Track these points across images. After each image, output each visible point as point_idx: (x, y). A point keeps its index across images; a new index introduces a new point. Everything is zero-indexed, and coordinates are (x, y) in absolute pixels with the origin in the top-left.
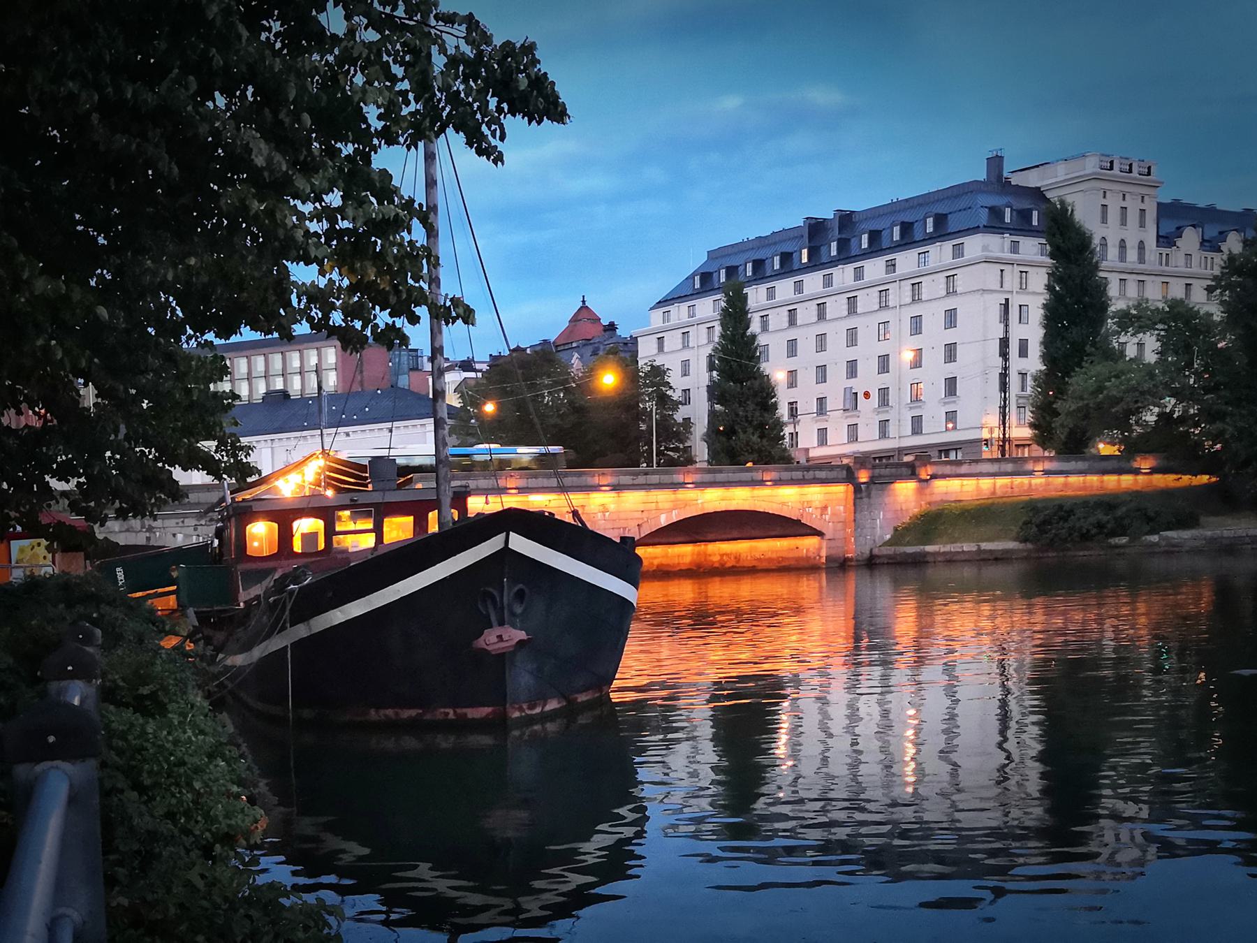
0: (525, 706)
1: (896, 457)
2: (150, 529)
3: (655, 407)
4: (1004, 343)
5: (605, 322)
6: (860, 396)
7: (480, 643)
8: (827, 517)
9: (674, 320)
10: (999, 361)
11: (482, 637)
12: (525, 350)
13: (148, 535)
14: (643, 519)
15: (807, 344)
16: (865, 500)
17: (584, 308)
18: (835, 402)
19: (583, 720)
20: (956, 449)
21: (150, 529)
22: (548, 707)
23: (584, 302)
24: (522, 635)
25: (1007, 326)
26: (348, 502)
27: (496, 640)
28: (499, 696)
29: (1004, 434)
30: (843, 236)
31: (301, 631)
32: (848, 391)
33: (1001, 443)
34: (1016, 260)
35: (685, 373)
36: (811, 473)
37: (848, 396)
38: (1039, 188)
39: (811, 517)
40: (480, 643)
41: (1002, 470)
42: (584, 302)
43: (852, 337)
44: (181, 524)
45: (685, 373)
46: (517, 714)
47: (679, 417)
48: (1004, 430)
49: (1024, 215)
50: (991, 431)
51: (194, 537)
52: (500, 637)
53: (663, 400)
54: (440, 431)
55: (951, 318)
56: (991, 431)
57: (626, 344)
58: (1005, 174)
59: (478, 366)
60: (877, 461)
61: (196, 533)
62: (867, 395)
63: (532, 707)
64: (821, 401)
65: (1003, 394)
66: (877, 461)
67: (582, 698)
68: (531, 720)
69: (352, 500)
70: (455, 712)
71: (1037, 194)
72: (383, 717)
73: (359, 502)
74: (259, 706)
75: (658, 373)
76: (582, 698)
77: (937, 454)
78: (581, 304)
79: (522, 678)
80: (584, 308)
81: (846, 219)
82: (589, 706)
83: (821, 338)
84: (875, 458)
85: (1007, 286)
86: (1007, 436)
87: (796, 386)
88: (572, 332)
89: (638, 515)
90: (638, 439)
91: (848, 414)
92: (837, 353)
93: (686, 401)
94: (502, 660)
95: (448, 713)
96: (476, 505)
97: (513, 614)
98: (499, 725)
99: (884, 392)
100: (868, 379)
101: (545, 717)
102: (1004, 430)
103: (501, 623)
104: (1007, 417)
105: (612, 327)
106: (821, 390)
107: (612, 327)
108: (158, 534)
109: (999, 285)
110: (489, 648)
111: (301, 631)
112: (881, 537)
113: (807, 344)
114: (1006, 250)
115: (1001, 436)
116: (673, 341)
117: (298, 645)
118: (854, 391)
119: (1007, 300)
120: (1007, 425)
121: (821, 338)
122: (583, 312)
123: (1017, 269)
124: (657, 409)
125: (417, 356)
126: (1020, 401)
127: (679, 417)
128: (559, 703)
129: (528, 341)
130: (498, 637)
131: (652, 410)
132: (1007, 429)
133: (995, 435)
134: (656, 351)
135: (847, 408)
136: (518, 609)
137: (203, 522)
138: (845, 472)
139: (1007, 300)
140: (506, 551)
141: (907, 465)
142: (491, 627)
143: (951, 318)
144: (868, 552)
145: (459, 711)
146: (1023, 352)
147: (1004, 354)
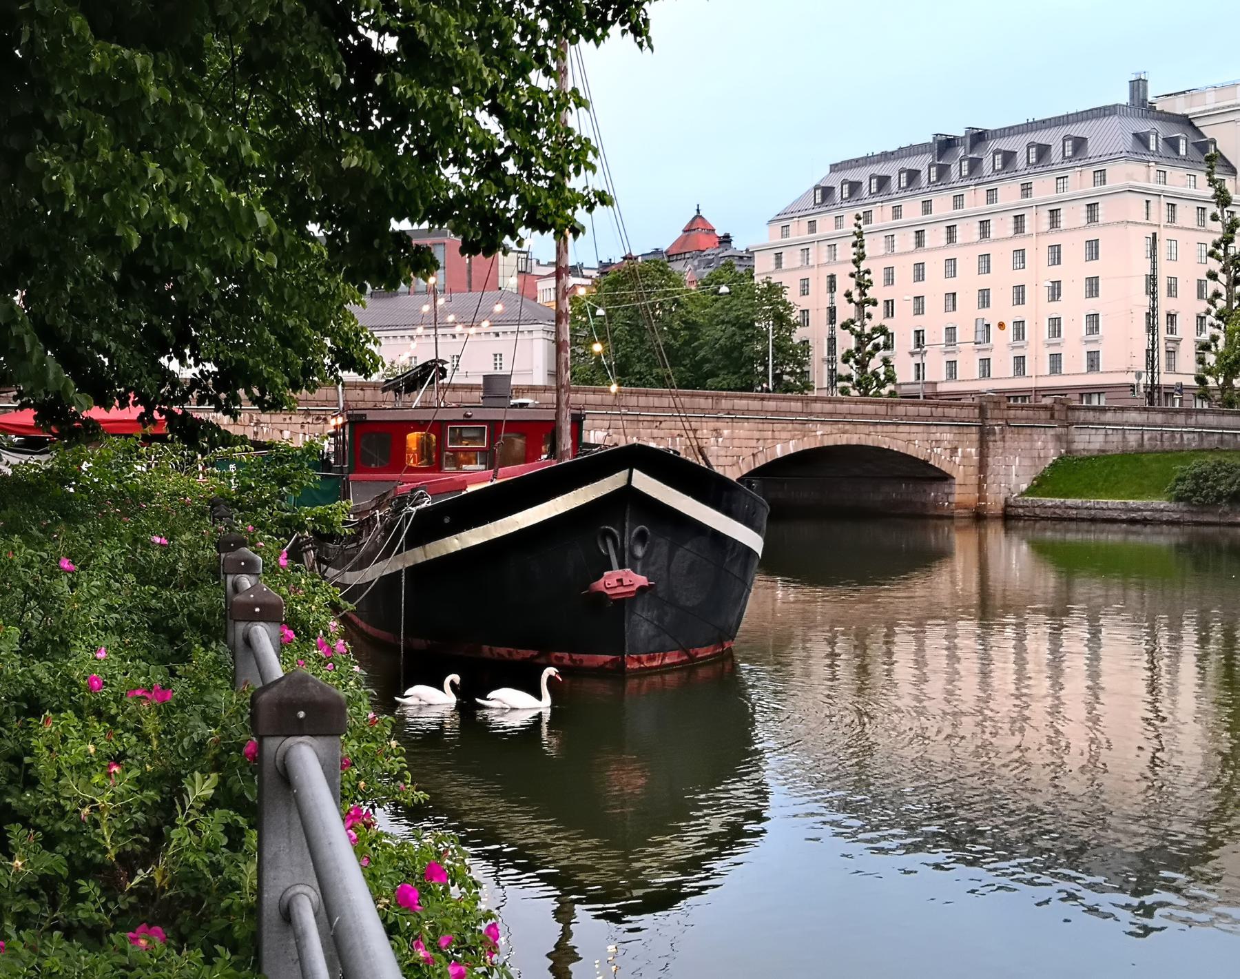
0: (644, 657)
1: (1032, 398)
2: (258, 423)
3: (771, 328)
4: (1152, 280)
5: (720, 233)
6: (994, 328)
7: (600, 585)
8: (958, 460)
9: (793, 237)
10: (1147, 300)
11: (602, 580)
12: (636, 258)
13: (255, 429)
14: (758, 448)
15: (935, 268)
16: (1000, 444)
17: (698, 216)
18: (965, 334)
19: (702, 673)
20: (1099, 394)
21: (258, 423)
22: (667, 661)
23: (698, 210)
24: (642, 580)
25: (1154, 262)
26: (461, 418)
27: (615, 584)
28: (617, 644)
29: (1153, 381)
30: (975, 155)
31: (419, 555)
32: (980, 322)
33: (1149, 390)
34: (1163, 191)
35: (804, 292)
36: (940, 409)
37: (980, 327)
38: (1187, 116)
39: (939, 459)
40: (600, 585)
41: (1150, 420)
42: (698, 210)
43: (985, 262)
44: (288, 421)
45: (804, 292)
46: (636, 665)
47: (796, 338)
48: (1153, 376)
49: (1172, 144)
50: (1139, 375)
51: (301, 435)
52: (620, 581)
53: (781, 319)
54: (563, 354)
55: (1093, 250)
56: (1139, 375)
57: (741, 258)
58: (1150, 99)
59: (585, 272)
60: (1012, 402)
61: (303, 431)
62: (1001, 325)
63: (651, 659)
64: (951, 332)
65: (1151, 337)
66: (1012, 402)
67: (702, 652)
68: (651, 671)
69: (465, 415)
70: (571, 658)
71: (1186, 122)
72: (496, 656)
73: (472, 418)
74: (370, 630)
75: (774, 290)
76: (702, 652)
77: (1077, 397)
78: (695, 213)
79: (642, 625)
80: (698, 216)
81: (978, 138)
82: (706, 662)
83: (951, 263)
84: (1009, 398)
85: (1154, 219)
86: (1156, 383)
87: (923, 313)
88: (684, 242)
89: (754, 443)
90: (751, 360)
91: (978, 346)
92: (968, 282)
93: (805, 322)
94: (621, 606)
95: (562, 658)
96: (595, 435)
97: (634, 558)
98: (617, 673)
99: (1019, 326)
100: (1002, 309)
101: (664, 670)
102: (1153, 376)
103: (622, 566)
104: (1156, 363)
105: (726, 239)
106: (951, 319)
107: (726, 239)
108: (265, 429)
109: (1145, 217)
110: (608, 592)
111: (419, 555)
112: (1018, 485)
113: (935, 268)
114: (1152, 180)
115: (1149, 382)
116: (792, 258)
117: (416, 571)
118: (986, 322)
119: (1154, 234)
120: (1156, 370)
121: (951, 263)
122: (698, 220)
123: (1164, 201)
124: (773, 330)
125: (527, 259)
126: (1169, 345)
127: (798, 336)
128: (679, 656)
129: (640, 248)
130: (618, 580)
131: (768, 330)
132: (1156, 375)
133: (1143, 381)
134: (773, 267)
135: (978, 340)
136: (639, 552)
137: (310, 420)
138: (977, 411)
139: (1154, 234)
140: (628, 493)
141: (1045, 408)
142: (611, 569)
143: (1093, 250)
144: (1003, 502)
145: (575, 656)
146: (1172, 291)
147: (1153, 294)
